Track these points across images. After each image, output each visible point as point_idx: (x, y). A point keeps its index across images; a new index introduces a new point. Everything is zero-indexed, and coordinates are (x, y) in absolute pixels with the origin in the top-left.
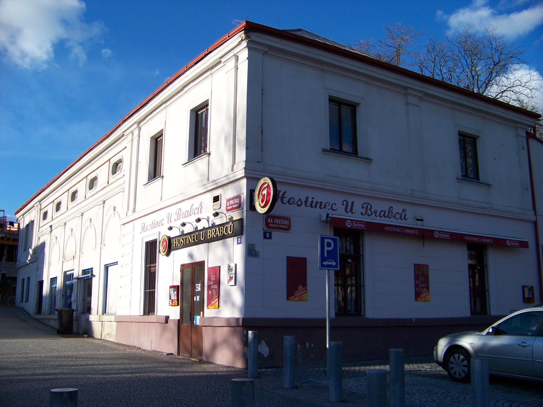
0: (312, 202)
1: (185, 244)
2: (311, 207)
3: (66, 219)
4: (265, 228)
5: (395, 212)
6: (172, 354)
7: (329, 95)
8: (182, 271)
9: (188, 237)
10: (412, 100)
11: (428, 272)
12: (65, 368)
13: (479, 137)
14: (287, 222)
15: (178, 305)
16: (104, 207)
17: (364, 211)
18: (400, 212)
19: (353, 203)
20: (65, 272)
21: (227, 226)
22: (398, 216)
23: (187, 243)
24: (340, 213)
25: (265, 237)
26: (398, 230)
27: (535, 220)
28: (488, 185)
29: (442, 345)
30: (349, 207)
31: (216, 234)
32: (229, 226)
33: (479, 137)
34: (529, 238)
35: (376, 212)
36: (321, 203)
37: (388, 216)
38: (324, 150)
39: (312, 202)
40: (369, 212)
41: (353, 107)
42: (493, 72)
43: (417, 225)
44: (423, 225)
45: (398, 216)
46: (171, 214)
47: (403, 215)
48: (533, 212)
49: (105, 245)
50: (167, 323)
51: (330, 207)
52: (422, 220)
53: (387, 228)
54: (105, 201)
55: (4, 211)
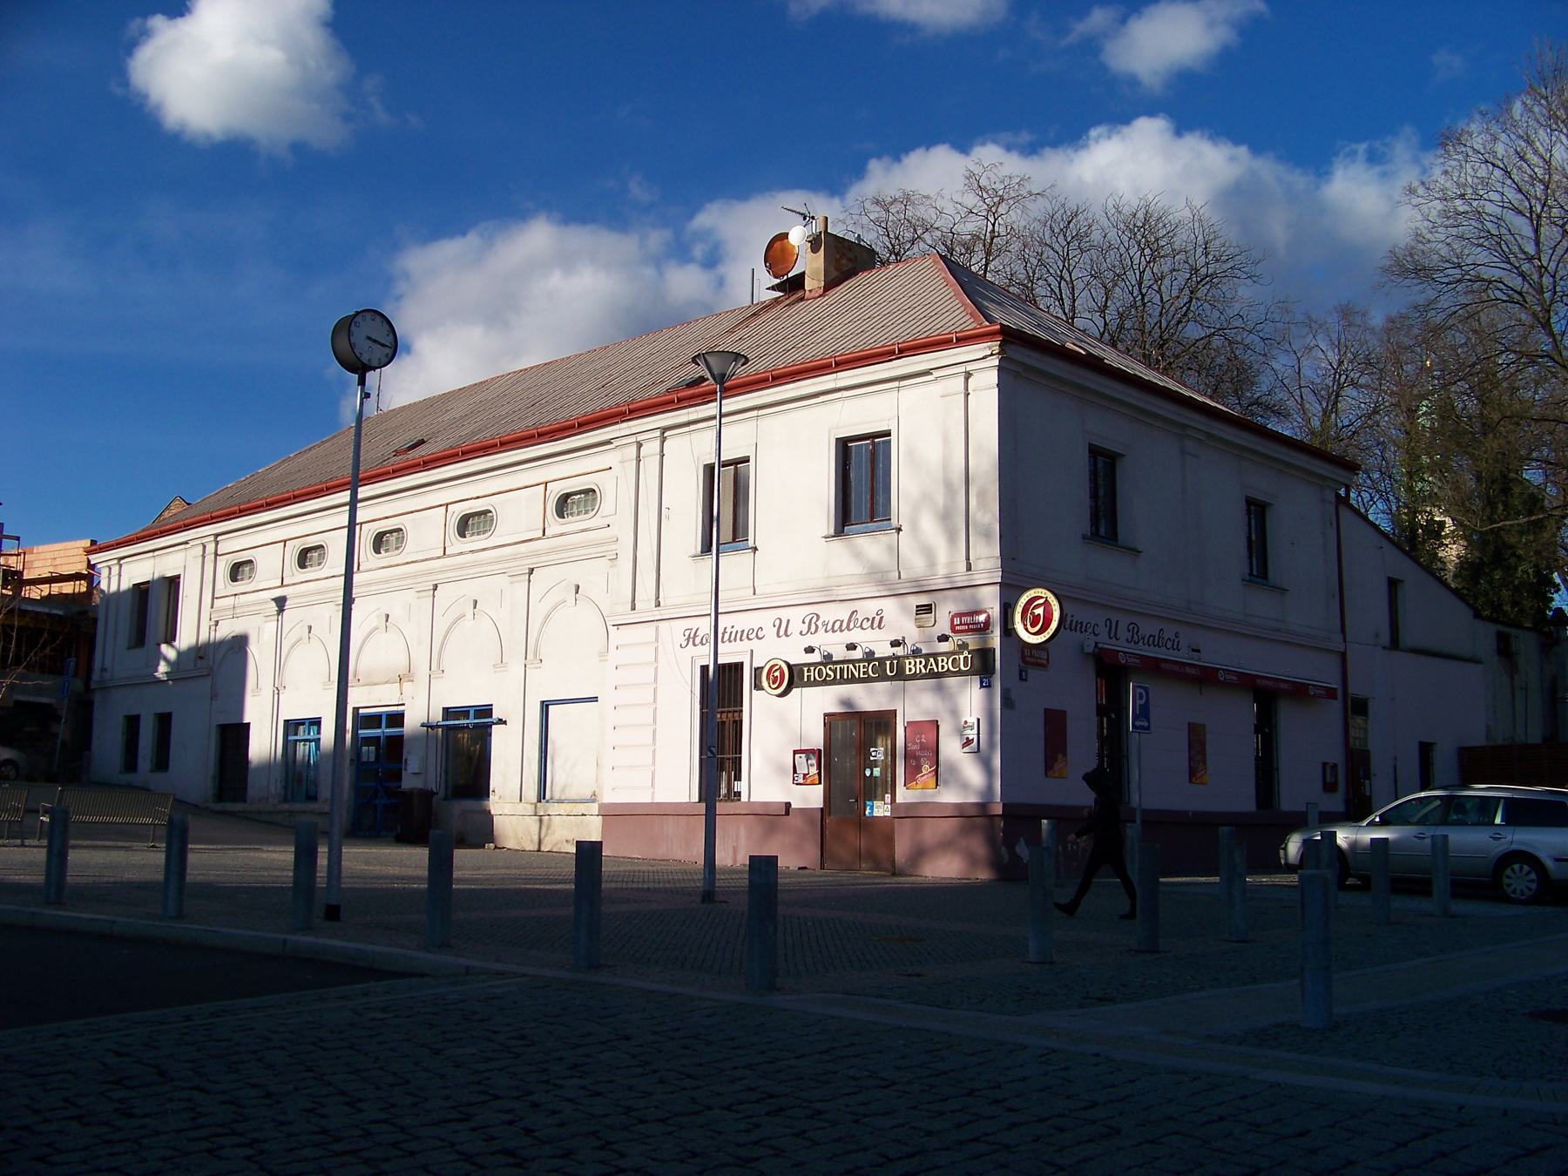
0: (1072, 621)
1: (838, 677)
4: (1022, 664)
6: (806, 868)
7: (1090, 444)
8: (828, 726)
9: (848, 667)
11: (1205, 736)
12: (1070, 845)
13: (1271, 504)
15: (820, 783)
16: (529, 581)
17: (1129, 635)
18: (1156, 633)
19: (1117, 622)
21: (957, 657)
22: (1169, 644)
23: (846, 677)
25: (1021, 679)
26: (1176, 668)
27: (1342, 650)
29: (1294, 846)
30: (1113, 634)
31: (929, 667)
32: (962, 657)
35: (1143, 638)
39: (1072, 621)
43: (1192, 659)
44: (1200, 660)
45: (1169, 644)
46: (788, 621)
49: (541, 660)
50: (788, 815)
51: (1090, 630)
52: (1198, 651)
54: (533, 569)
55: (18, 539)
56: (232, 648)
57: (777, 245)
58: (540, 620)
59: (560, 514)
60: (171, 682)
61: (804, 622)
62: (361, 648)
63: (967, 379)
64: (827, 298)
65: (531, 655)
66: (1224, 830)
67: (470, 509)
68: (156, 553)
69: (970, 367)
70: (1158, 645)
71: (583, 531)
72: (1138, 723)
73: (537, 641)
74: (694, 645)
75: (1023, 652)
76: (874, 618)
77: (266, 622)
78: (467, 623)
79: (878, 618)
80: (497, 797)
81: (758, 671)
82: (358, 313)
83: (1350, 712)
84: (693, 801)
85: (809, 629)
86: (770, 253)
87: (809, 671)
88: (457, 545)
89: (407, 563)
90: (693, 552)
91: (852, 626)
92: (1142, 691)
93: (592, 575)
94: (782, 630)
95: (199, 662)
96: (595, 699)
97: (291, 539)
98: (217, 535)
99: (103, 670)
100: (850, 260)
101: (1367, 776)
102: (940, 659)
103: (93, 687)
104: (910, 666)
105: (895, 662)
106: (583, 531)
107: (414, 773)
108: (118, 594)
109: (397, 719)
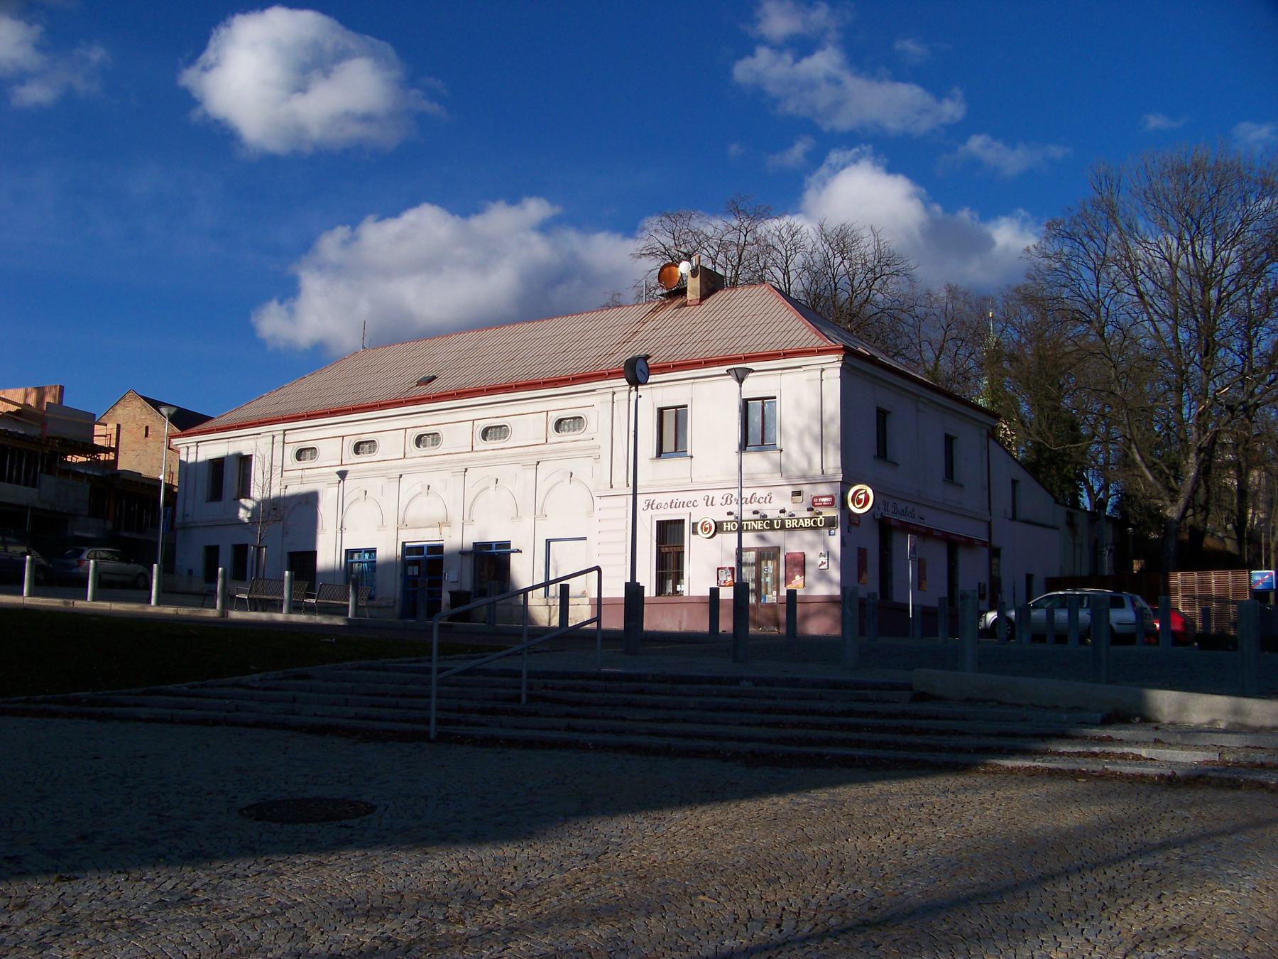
3: (405, 470)
13: (956, 438)
18: (904, 509)
20: (404, 543)
33: (956, 438)
44: (923, 523)
46: (713, 498)
56: (300, 503)
57: (666, 270)
58: (544, 495)
59: (557, 429)
60: (250, 524)
61: (723, 498)
62: (472, 505)
63: (822, 372)
64: (703, 307)
65: (539, 513)
67: (491, 424)
68: (231, 440)
69: (824, 366)
71: (574, 441)
72: (912, 555)
73: (543, 506)
74: (652, 509)
75: (849, 517)
76: (766, 498)
77: (329, 487)
78: (492, 491)
79: (768, 498)
81: (695, 525)
84: (652, 596)
85: (726, 502)
86: (662, 274)
87: (727, 525)
88: (480, 444)
89: (444, 454)
90: (651, 457)
93: (583, 468)
94: (709, 502)
96: (585, 539)
98: (285, 430)
99: (185, 515)
100: (712, 282)
101: (1000, 591)
102: (806, 520)
103: (176, 526)
104: (788, 523)
105: (780, 521)
106: (574, 441)
107: (452, 582)
108: (196, 464)
109: (372, 551)
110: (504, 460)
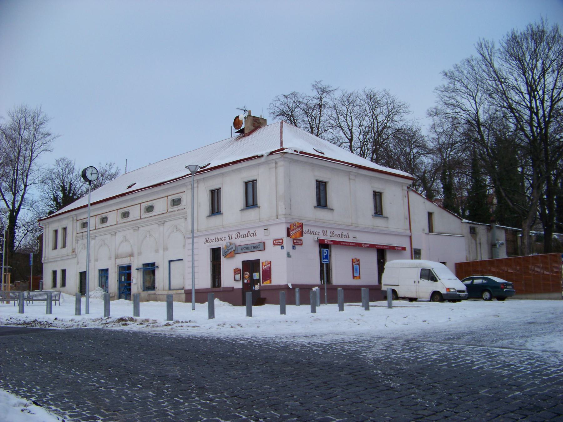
0: (310, 232)
2: (310, 234)
5: (344, 234)
10: (352, 177)
14: (301, 242)
17: (331, 235)
18: (346, 234)
19: (326, 231)
22: (345, 236)
24: (322, 237)
25: (293, 249)
26: (346, 244)
28: (387, 218)
30: (325, 234)
34: (407, 245)
35: (336, 235)
36: (314, 232)
37: (341, 237)
38: (315, 207)
39: (310, 232)
40: (333, 235)
41: (325, 184)
42: (464, 115)
45: (345, 236)
47: (348, 236)
48: (410, 231)
53: (342, 243)
66: (339, 289)
70: (341, 237)
74: (208, 243)
75: (293, 241)
80: (157, 290)
82: (88, 167)
83: (4, 255)
91: (248, 236)
92: (326, 251)
95: (73, 253)
96: (182, 260)
97: (170, 196)
110: (104, 233)
